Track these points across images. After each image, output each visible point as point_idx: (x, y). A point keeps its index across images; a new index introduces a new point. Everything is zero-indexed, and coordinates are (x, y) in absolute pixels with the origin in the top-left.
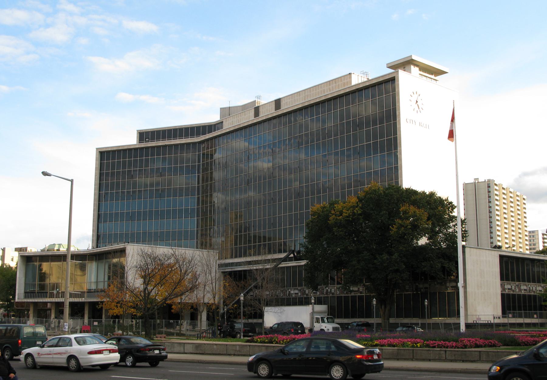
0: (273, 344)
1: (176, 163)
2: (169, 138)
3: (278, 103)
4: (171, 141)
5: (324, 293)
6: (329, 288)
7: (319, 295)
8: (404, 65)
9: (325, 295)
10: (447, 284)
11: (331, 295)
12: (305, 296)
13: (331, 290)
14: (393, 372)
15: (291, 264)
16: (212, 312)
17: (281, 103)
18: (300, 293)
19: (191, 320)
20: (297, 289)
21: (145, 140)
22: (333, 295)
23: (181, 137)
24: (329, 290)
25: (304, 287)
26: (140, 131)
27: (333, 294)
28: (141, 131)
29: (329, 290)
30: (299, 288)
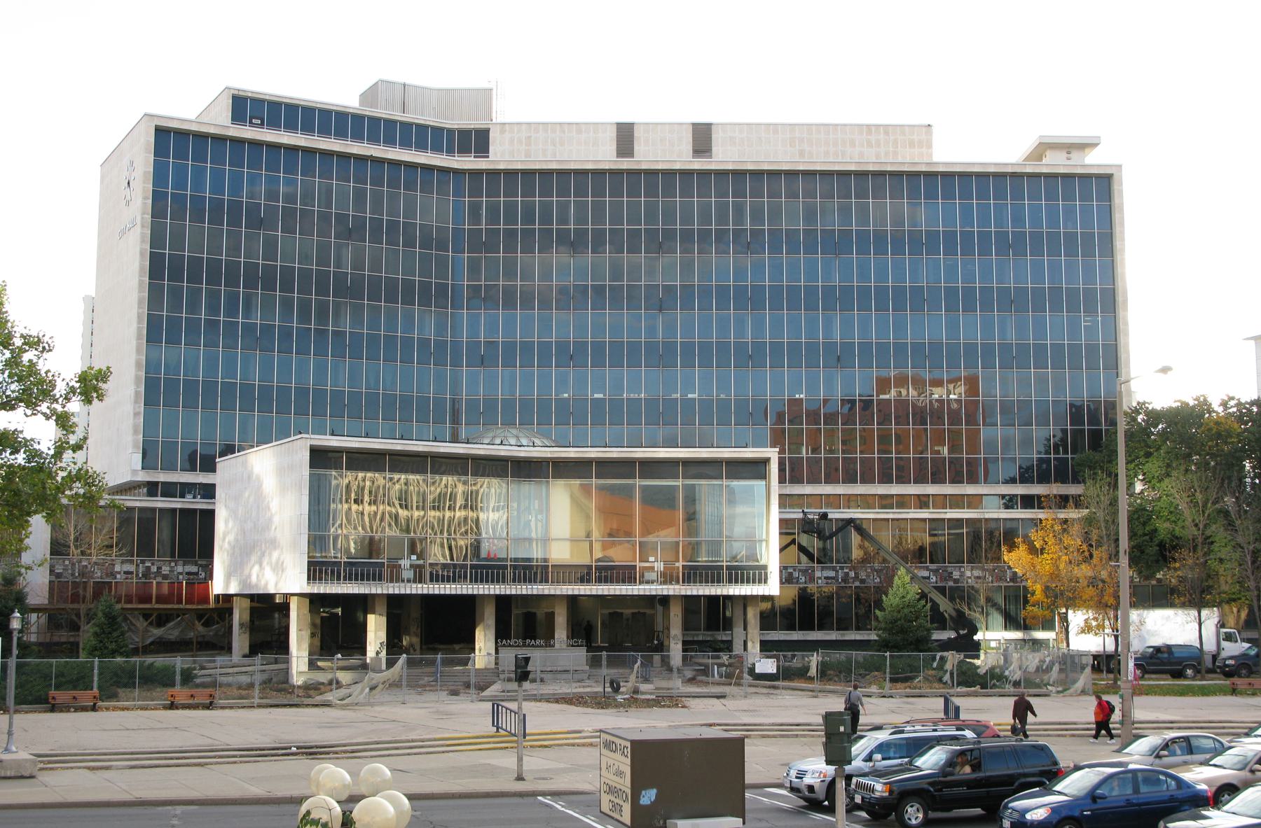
0: (1186, 677)
1: (511, 218)
2: (325, 131)
3: (702, 136)
4: (362, 145)
5: (1006, 580)
6: (153, 564)
7: (936, 583)
8: (1069, 148)
9: (1008, 582)
10: (116, 566)
11: (857, 584)
12: (951, 584)
13: (159, 568)
14: (1046, 738)
15: (840, 514)
16: (880, 610)
17: (714, 136)
18: (934, 578)
19: (720, 630)
20: (927, 569)
21: (251, 122)
22: (958, 583)
23: (341, 134)
24: (154, 569)
25: (947, 565)
26: (236, 92)
27: (863, 581)
28: (241, 93)
29: (154, 569)
30: (933, 566)
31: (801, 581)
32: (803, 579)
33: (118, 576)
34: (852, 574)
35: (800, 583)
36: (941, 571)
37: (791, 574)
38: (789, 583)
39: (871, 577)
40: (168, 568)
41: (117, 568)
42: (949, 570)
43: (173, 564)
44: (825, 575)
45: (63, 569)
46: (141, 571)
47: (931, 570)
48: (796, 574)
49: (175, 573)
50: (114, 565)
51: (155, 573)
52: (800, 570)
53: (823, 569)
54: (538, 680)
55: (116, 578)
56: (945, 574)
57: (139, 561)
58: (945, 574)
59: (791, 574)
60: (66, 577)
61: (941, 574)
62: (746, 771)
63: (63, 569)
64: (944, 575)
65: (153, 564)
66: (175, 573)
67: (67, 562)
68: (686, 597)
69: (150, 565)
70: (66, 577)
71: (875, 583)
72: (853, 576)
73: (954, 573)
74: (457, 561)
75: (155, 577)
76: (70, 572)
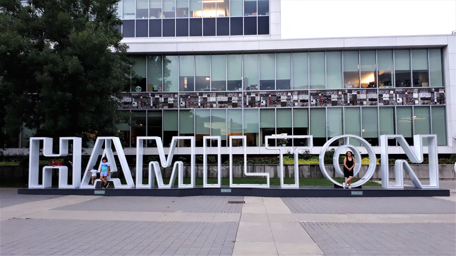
18: (136, 103)
29: (162, 100)
31: (262, 104)
32: (264, 102)
33: (417, 102)
34: (162, 100)
35: (262, 106)
36: (141, 97)
37: (253, 98)
38: (252, 107)
39: (394, 99)
40: (388, 95)
41: (415, 95)
42: (278, 94)
43: (289, 94)
44: (370, 97)
45: (174, 101)
46: (348, 99)
47: (134, 97)
48: (258, 99)
49: (292, 101)
50: (412, 93)
51: (163, 103)
52: (261, 95)
53: (419, 91)
54: (219, 143)
55: (414, 104)
56: (274, 99)
57: (246, 93)
58: (274, 99)
59: (253, 98)
60: (392, 104)
61: (406, 96)
62: (259, 154)
63: (174, 101)
64: (273, 99)
65: (161, 96)
66: (292, 101)
67: (392, 92)
68: (162, 117)
69: (254, 96)
70: (392, 104)
71: (398, 104)
72: (163, 101)
73: (282, 97)
74: (293, 89)
75: (163, 106)
76: (343, 100)
